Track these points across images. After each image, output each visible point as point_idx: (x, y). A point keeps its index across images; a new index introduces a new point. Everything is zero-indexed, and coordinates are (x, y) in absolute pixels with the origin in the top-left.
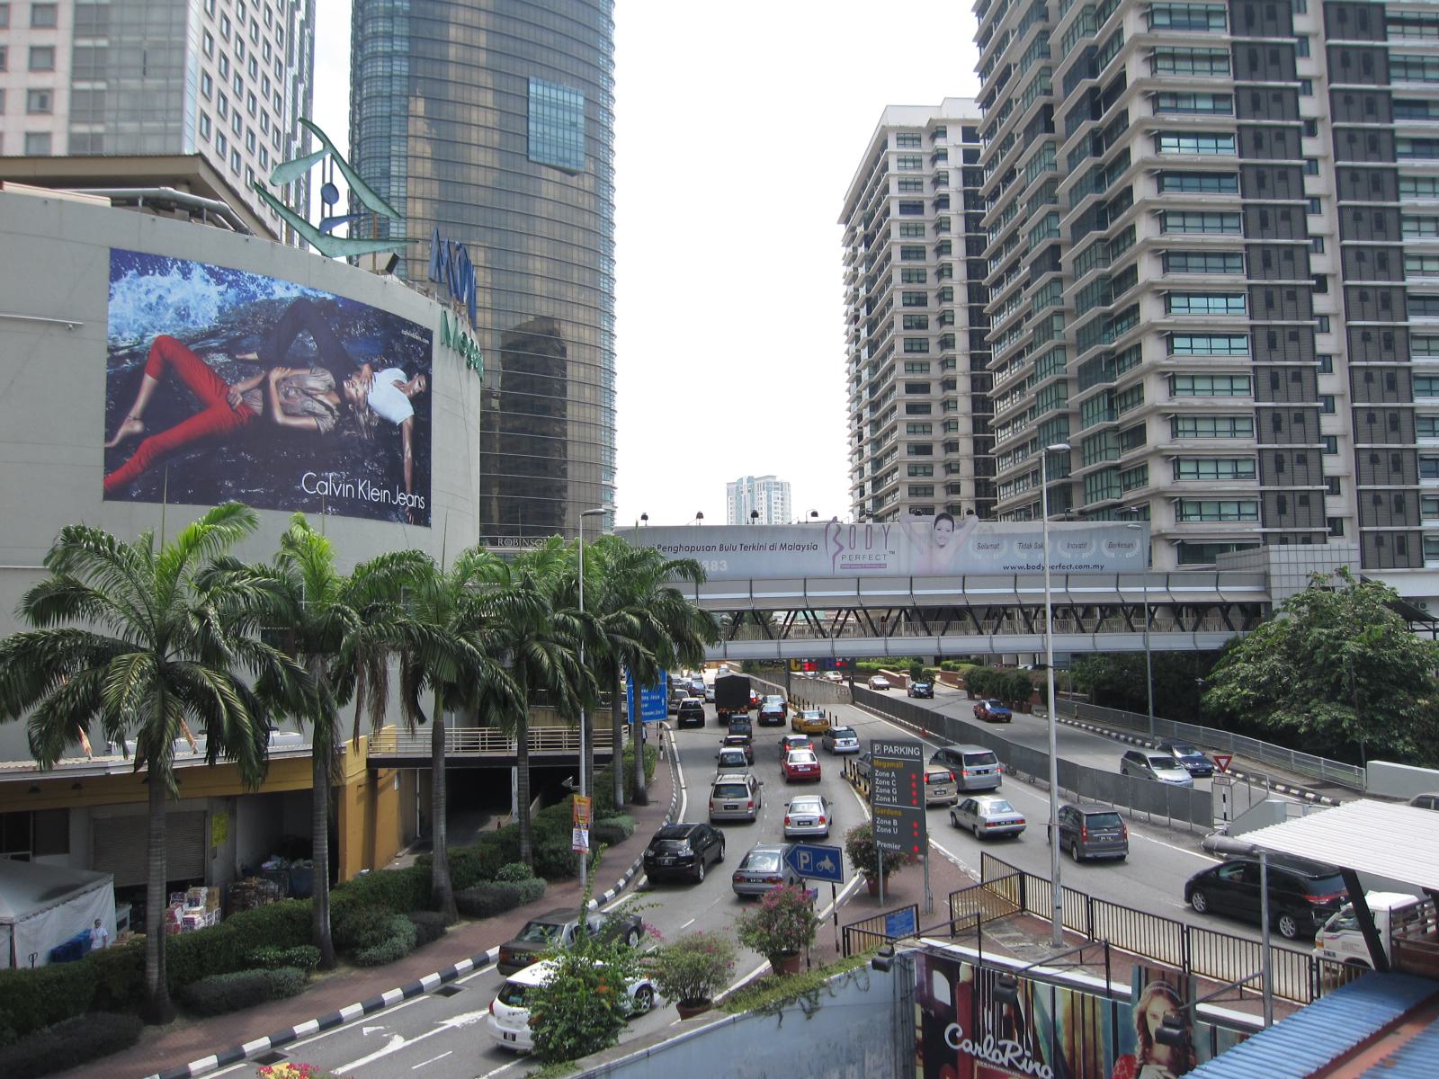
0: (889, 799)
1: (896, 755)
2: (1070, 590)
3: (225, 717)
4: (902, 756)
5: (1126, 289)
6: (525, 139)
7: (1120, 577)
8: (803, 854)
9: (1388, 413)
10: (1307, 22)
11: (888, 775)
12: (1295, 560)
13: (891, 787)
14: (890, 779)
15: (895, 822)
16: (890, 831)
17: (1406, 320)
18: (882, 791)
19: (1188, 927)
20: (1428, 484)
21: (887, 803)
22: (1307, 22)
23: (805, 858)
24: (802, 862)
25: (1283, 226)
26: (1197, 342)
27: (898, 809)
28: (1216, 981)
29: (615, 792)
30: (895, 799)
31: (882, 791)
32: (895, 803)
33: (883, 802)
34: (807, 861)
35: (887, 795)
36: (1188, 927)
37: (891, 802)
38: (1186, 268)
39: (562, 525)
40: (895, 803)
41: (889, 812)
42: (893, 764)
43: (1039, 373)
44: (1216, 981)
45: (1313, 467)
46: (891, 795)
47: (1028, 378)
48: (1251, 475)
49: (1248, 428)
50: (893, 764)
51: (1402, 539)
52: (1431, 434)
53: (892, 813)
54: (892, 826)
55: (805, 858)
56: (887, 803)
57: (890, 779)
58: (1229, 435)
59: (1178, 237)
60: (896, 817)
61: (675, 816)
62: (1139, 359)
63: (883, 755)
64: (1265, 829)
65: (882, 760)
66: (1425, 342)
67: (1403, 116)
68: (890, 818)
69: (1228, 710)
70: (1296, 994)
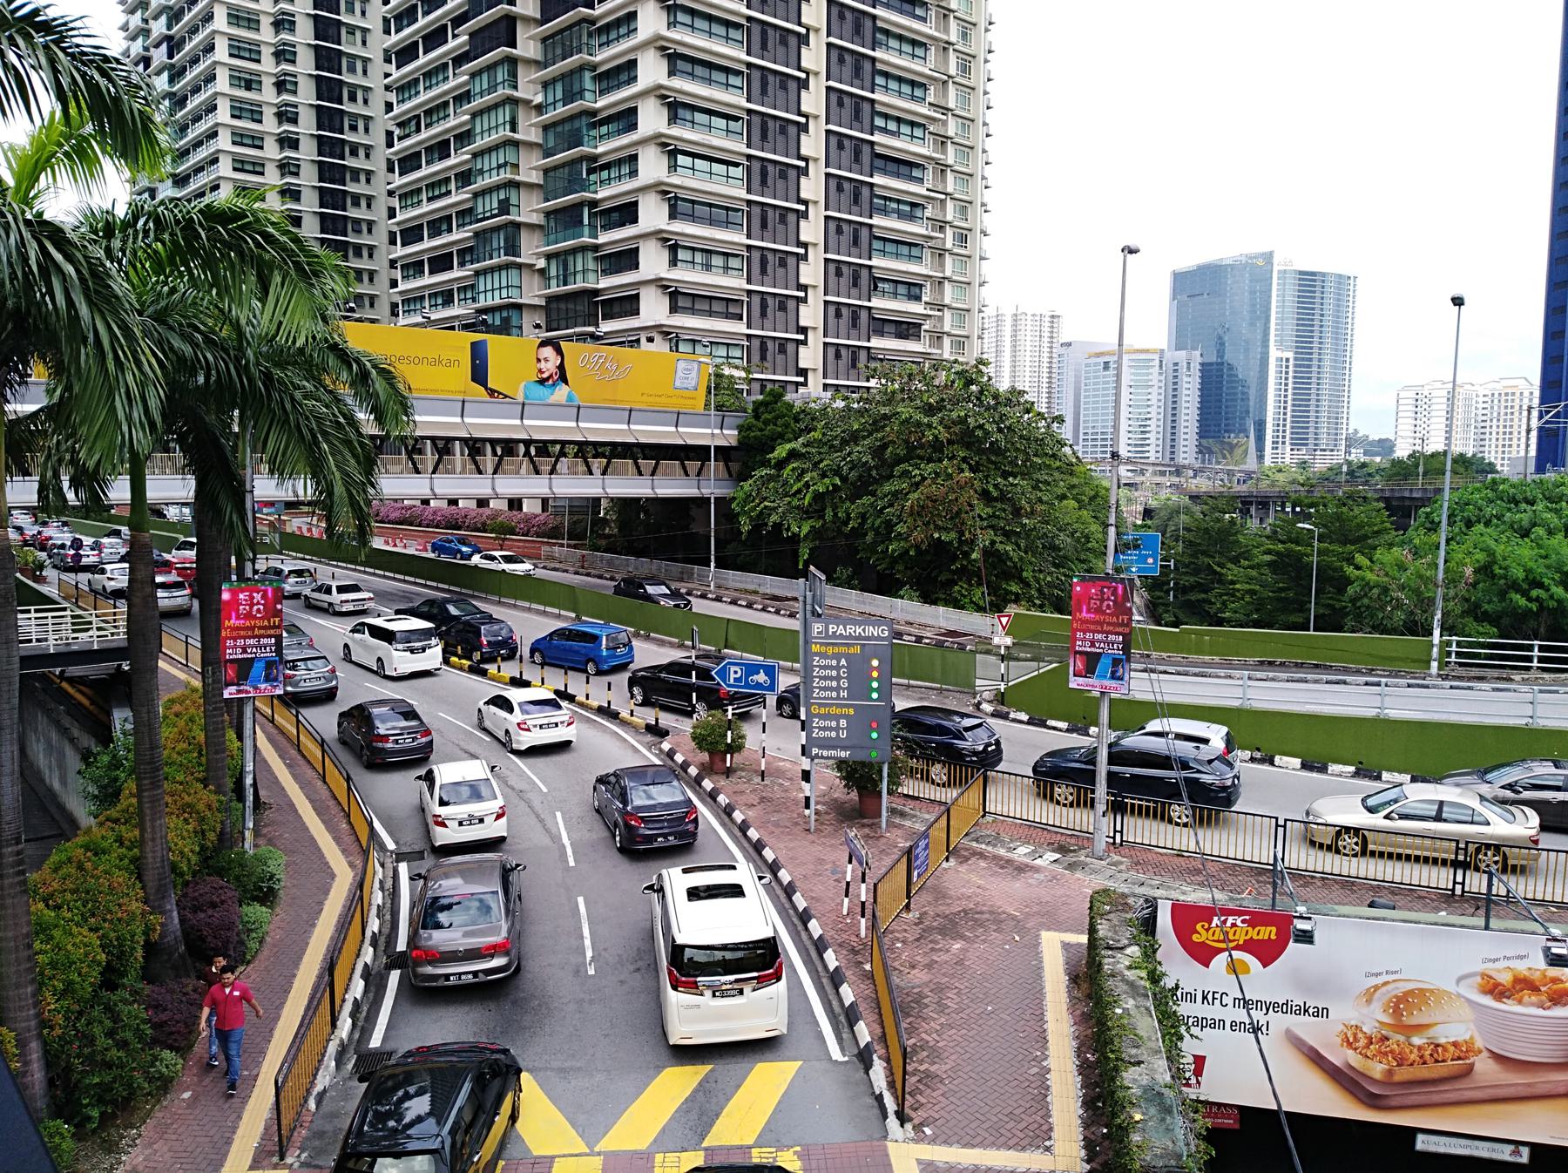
0: (834, 694)
1: (850, 637)
4: (860, 638)
5: (618, 87)
6: (1470, 819)
8: (733, 669)
11: (834, 663)
13: (838, 678)
14: (838, 668)
15: (843, 723)
16: (833, 734)
18: (824, 683)
21: (832, 699)
23: (736, 672)
24: (733, 676)
29: (352, 422)
30: (844, 694)
31: (824, 683)
32: (844, 699)
33: (825, 698)
34: (738, 675)
37: (838, 698)
40: (844, 699)
41: (834, 710)
42: (844, 649)
43: (478, 130)
46: (838, 689)
47: (424, 74)
50: (844, 649)
53: (839, 711)
54: (837, 729)
55: (736, 672)
57: (838, 668)
59: (689, 276)
60: (846, 716)
61: (194, 690)
62: (634, 173)
63: (827, 637)
67: (885, 172)
68: (837, 718)
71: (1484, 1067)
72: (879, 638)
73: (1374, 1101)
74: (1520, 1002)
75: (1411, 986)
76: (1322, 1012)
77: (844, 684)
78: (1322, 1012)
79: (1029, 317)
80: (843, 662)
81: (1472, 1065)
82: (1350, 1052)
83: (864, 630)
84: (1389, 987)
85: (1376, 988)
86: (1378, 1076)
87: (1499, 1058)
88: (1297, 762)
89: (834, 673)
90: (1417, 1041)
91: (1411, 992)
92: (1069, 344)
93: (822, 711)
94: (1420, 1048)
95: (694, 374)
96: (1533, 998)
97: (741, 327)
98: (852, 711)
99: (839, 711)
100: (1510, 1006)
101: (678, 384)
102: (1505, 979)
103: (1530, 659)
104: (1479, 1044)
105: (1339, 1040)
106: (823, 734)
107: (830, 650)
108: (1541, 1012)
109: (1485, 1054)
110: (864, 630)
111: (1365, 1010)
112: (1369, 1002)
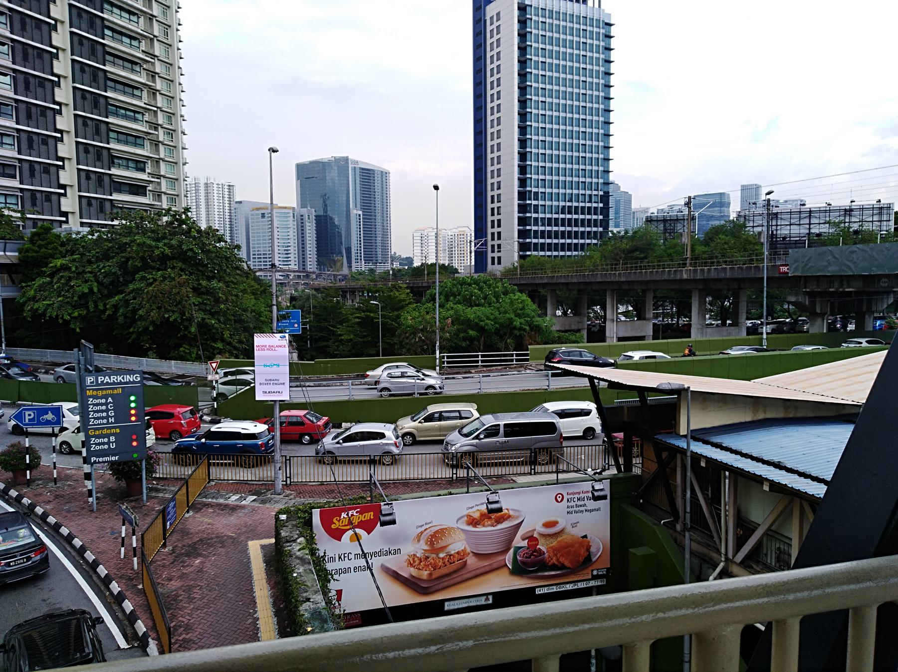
0: (105, 421)
1: (114, 383)
4: (121, 383)
9: (41, 137)
10: (60, 11)
13: (107, 411)
14: (106, 404)
15: (112, 439)
16: (106, 447)
17: (106, 91)
20: (8, 152)
22: (60, 11)
27: (115, 428)
33: (98, 424)
37: (108, 423)
39: (516, 268)
40: (112, 423)
41: (105, 432)
42: (110, 392)
46: (107, 417)
49: (14, 201)
50: (110, 392)
51: (99, 150)
53: (109, 431)
57: (106, 404)
65: (93, 390)
66: (131, 89)
69: (728, 322)
71: (471, 561)
72: (134, 382)
73: (424, 591)
74: (484, 526)
76: (397, 551)
78: (397, 551)
79: (215, 186)
80: (110, 400)
81: (466, 562)
82: (412, 569)
83: (123, 378)
84: (427, 531)
85: (422, 533)
86: (425, 577)
87: (476, 555)
90: (442, 555)
91: (437, 532)
92: (240, 202)
93: (97, 433)
94: (443, 559)
97: (15, 183)
98: (118, 430)
99: (109, 431)
100: (480, 529)
102: (477, 515)
103: (512, 360)
104: (468, 550)
105: (406, 564)
107: (100, 393)
108: (492, 528)
109: (471, 554)
111: (417, 546)
112: (419, 541)
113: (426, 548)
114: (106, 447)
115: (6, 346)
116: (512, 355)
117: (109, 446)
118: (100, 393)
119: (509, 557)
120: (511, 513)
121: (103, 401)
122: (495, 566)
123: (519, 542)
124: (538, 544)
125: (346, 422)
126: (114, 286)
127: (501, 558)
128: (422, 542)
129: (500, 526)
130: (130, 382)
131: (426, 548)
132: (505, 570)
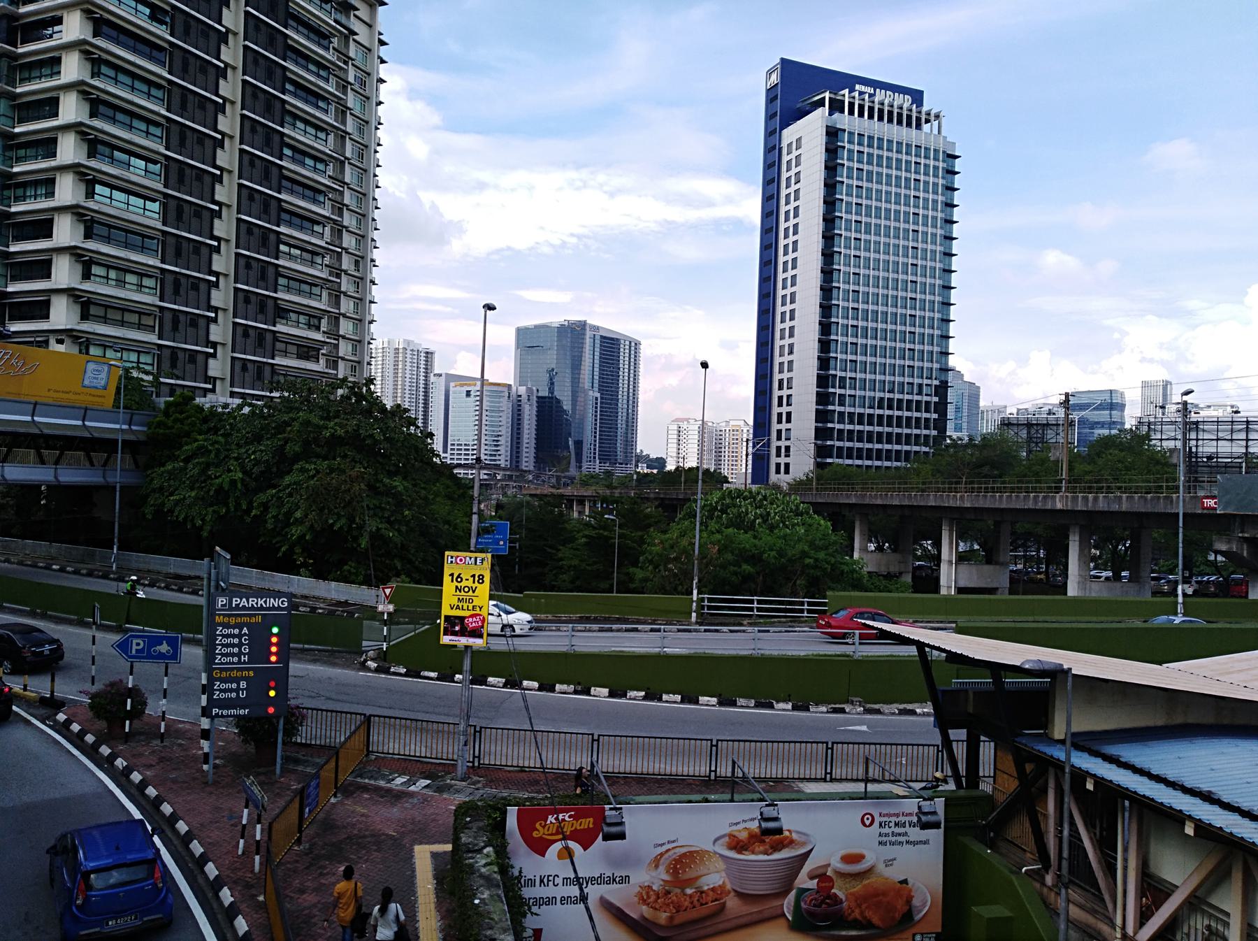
0: (235, 660)
2: (35, 418)
3: (844, 933)
4: (262, 608)
7: (38, 406)
12: (1244, 443)
14: (240, 636)
15: (243, 684)
16: (234, 695)
19: (481, 728)
21: (233, 663)
25: (198, 113)
26: (117, 195)
27: (248, 669)
28: (512, 769)
31: (225, 650)
35: (233, 655)
36: (481, 728)
37: (239, 662)
38: (114, 121)
40: (245, 663)
44: (512, 769)
45: (202, 333)
46: (239, 655)
48: (151, 329)
52: (103, 320)
53: (239, 674)
56: (233, 663)
58: (135, 288)
60: (243, 678)
63: (231, 608)
64: (959, 652)
70: (925, 775)
71: (732, 903)
74: (753, 853)
75: (683, 850)
76: (625, 879)
77: (245, 649)
78: (625, 879)
80: (245, 630)
81: (724, 904)
83: (265, 602)
84: (670, 853)
85: (662, 855)
87: (740, 895)
88: (605, 691)
89: (236, 641)
90: (689, 891)
91: (684, 855)
93: (224, 675)
94: (691, 896)
95: (104, 375)
96: (762, 848)
99: (239, 674)
101: (86, 382)
104: (729, 887)
106: (223, 696)
107: (233, 620)
109: (732, 894)
110: (265, 602)
111: (654, 874)
112: (657, 866)
113: (667, 877)
114: (234, 695)
115: (119, 549)
116: (802, 604)
117: (238, 694)
118: (233, 620)
119: (789, 902)
120: (794, 836)
121: (236, 631)
122: (766, 914)
123: (804, 881)
124: (832, 887)
125: (562, 683)
126: (267, 477)
127: (776, 903)
128: (662, 868)
129: (776, 856)
130: (274, 608)
131: (667, 877)
132: (782, 921)
